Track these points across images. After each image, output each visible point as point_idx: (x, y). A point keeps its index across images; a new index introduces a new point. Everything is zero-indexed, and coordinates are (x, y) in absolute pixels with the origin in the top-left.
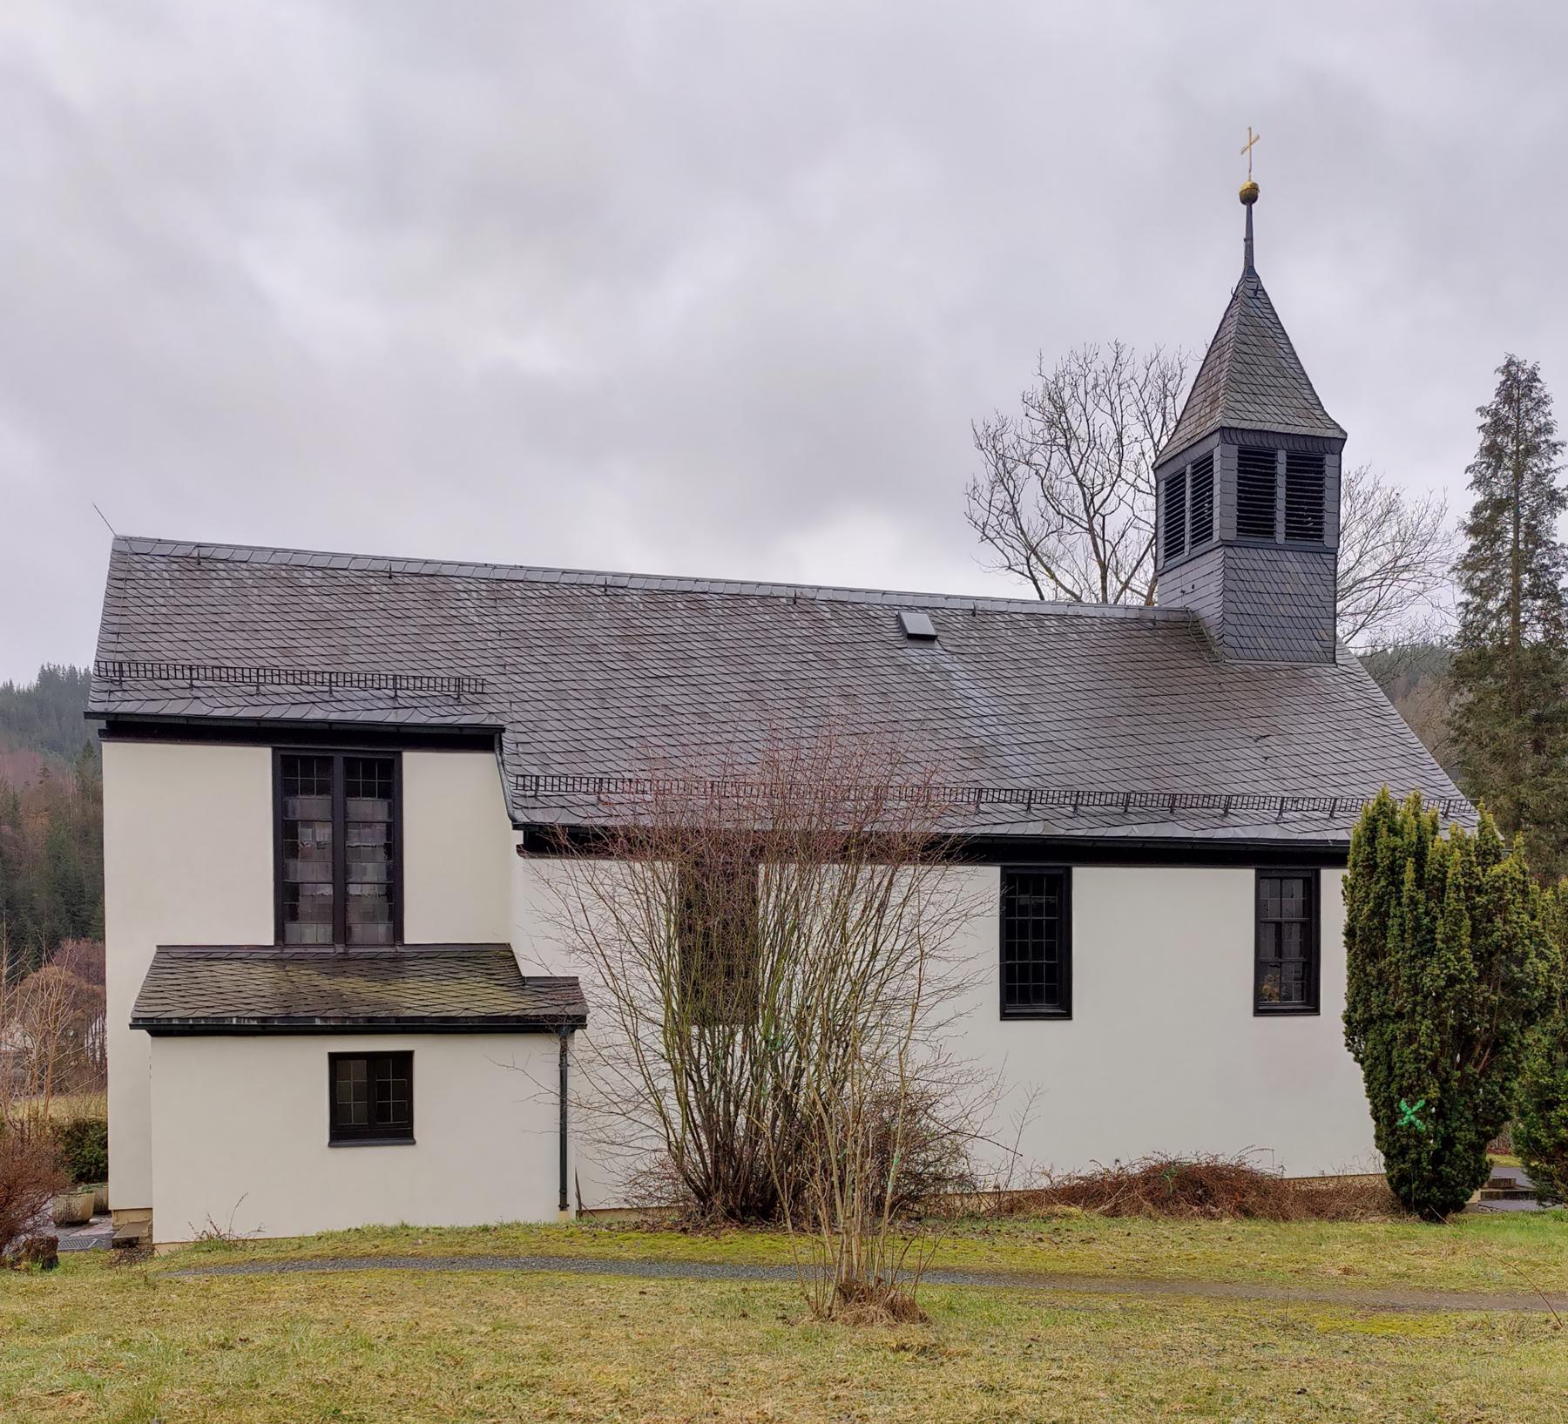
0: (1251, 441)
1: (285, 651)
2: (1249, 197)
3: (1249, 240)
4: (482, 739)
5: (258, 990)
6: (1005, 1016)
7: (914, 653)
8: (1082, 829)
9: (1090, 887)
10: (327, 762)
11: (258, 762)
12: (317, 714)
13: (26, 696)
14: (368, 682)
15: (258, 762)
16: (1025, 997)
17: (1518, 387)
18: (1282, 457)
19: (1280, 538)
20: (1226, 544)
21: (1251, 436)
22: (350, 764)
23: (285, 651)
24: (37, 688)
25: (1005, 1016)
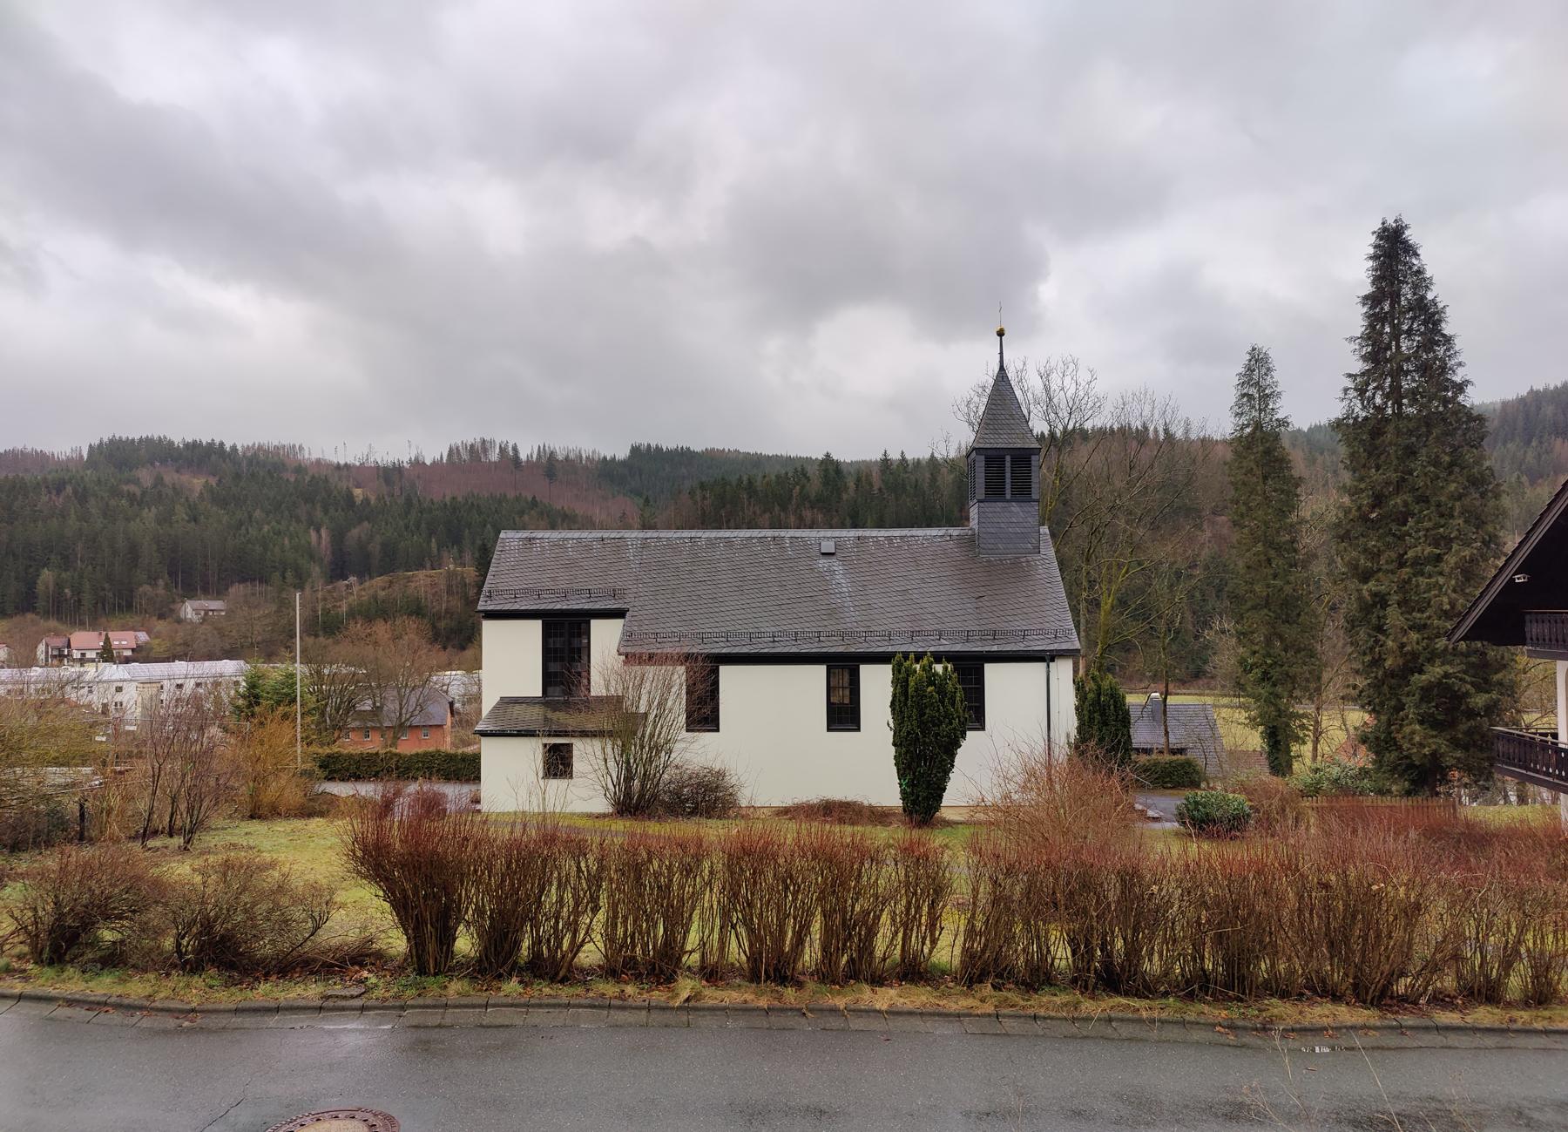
1: (553, 579)
2: (1001, 333)
4: (619, 614)
5: (534, 715)
6: (829, 730)
7: (823, 563)
11: (537, 625)
13: (623, 463)
14: (579, 592)
15: (537, 625)
16: (841, 722)
17: (1393, 248)
18: (1008, 458)
19: (1008, 496)
21: (590, 727)
23: (553, 579)
25: (829, 730)
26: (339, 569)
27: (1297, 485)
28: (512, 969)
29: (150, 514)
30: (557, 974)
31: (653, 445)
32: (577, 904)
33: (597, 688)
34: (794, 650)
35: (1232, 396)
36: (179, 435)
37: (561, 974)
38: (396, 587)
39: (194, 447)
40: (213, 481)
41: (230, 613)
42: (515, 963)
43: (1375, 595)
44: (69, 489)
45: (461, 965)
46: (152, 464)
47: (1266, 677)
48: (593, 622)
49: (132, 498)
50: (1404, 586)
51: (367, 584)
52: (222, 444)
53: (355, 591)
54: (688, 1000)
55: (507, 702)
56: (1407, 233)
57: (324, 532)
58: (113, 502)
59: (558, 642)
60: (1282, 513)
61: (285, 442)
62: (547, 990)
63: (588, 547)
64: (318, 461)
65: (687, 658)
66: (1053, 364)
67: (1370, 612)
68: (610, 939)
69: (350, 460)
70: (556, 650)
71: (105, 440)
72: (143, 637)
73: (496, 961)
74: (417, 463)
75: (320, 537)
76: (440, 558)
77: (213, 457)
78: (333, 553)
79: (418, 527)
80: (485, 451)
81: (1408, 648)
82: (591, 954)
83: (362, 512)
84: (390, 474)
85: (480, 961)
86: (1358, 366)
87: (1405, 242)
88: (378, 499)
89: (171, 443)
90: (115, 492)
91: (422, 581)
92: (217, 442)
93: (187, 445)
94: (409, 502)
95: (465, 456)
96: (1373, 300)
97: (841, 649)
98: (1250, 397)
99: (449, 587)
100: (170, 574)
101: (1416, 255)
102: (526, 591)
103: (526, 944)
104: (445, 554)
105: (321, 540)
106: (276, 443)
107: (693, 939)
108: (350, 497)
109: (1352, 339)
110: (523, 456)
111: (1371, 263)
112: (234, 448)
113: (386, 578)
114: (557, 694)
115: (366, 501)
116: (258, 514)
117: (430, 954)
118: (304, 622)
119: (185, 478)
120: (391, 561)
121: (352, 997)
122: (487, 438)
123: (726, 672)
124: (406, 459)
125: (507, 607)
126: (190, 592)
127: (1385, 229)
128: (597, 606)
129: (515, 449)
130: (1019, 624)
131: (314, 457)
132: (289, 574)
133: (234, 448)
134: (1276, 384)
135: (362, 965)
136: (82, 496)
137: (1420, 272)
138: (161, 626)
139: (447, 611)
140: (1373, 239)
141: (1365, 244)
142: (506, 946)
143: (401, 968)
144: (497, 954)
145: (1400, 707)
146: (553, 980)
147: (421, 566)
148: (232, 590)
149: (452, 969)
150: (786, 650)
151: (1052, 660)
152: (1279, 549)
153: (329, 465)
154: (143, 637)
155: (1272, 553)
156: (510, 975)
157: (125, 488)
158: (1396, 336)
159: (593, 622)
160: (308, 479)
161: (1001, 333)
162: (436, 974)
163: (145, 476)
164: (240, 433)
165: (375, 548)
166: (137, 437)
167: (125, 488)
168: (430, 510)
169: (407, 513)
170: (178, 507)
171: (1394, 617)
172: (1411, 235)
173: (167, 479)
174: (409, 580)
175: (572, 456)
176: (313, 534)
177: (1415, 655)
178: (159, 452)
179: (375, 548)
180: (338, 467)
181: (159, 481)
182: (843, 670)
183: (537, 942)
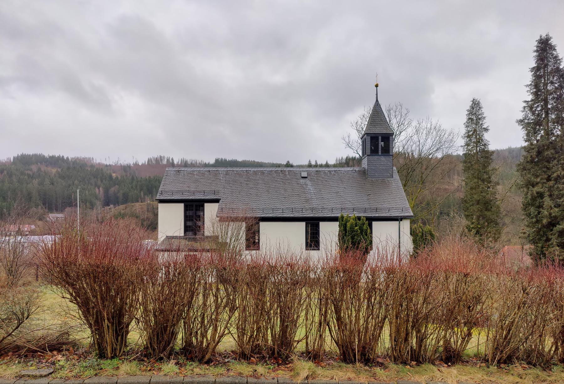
0: (372, 135)
1: (188, 187)
2: (377, 86)
3: (377, 94)
4: (217, 201)
7: (302, 181)
8: (321, 215)
10: (192, 206)
11: (182, 205)
12: (191, 198)
14: (199, 192)
15: (182, 205)
16: (311, 246)
17: (475, 106)
18: (380, 138)
19: (380, 154)
20: (368, 155)
22: (196, 206)
23: (188, 187)
24: (143, 165)
26: (107, 203)
27: (491, 155)
28: (170, 354)
29: (36, 182)
30: (203, 357)
31: (223, 158)
32: (217, 308)
33: (207, 233)
34: (292, 216)
35: (464, 119)
36: (47, 153)
37: (207, 357)
38: (128, 209)
39: (52, 157)
40: (59, 170)
41: (66, 219)
42: (172, 349)
43: (537, 193)
44: (5, 172)
45: (132, 351)
46: (37, 164)
47: (478, 232)
48: (206, 205)
49: (29, 176)
50: (550, 189)
51: (117, 208)
52: (63, 157)
53: (113, 210)
54: (307, 378)
55: (168, 238)
56: (552, 40)
57: (101, 189)
58: (22, 177)
59: (190, 213)
60: (485, 167)
61: (87, 157)
62: (197, 370)
63: (203, 174)
64: (99, 163)
65: (245, 219)
66: (391, 106)
67: (535, 202)
68: (242, 331)
69: (111, 163)
70: (190, 216)
71: (20, 155)
72: (33, 227)
73: (159, 348)
74: (136, 165)
75: (99, 191)
76: (144, 198)
77: (60, 161)
78: (104, 196)
79: (136, 187)
80: (161, 160)
81: (554, 214)
82: (228, 343)
83: (117, 182)
84: (126, 168)
85: (146, 348)
86: (530, 98)
87: (550, 45)
88: (121, 176)
89: (44, 156)
90: (22, 173)
91: (138, 206)
92: (61, 156)
93: (50, 157)
94: (133, 177)
95: (154, 162)
96: (536, 70)
97: (312, 215)
98: (472, 119)
99: (148, 209)
100: (43, 204)
101: (555, 49)
102: (178, 192)
103: (180, 336)
104: (146, 197)
105: (100, 192)
106: (83, 157)
107: (300, 333)
108: (111, 177)
109: (527, 86)
110: (175, 162)
111: (535, 54)
112: (68, 158)
113: (124, 206)
114: (190, 234)
115: (117, 178)
116: (76, 182)
117: (109, 343)
118: (80, 199)
119: (49, 169)
120: (126, 200)
121: (41, 376)
122: (162, 156)
123: (263, 225)
124: (132, 163)
125: (169, 198)
126: (51, 210)
127: (541, 40)
128: (207, 198)
129: (172, 159)
130: (386, 205)
131: (97, 162)
132: (88, 204)
133: (68, 158)
134: (483, 114)
135: (60, 351)
136: (10, 175)
137: (556, 57)
138: (40, 223)
139: (147, 218)
140: (536, 44)
141: (533, 45)
142: (166, 337)
143: (426, 317)
144: (159, 342)
145: (548, 240)
146: (201, 361)
147: (138, 201)
148: (66, 210)
149: (124, 354)
150: (288, 216)
151: (401, 220)
152: (483, 181)
153: (103, 165)
154: (33, 227)
155: (480, 183)
156: (169, 358)
157: (26, 172)
158: (546, 85)
159: (206, 205)
160: (95, 170)
162: (112, 358)
163: (34, 168)
164: (69, 153)
165: (120, 195)
166: (31, 154)
167: (26, 172)
168: (141, 181)
169: (132, 182)
170: (46, 179)
171: (547, 201)
172: (553, 42)
173: (42, 169)
174: (133, 206)
175: (193, 162)
176: (97, 190)
177: (556, 217)
178: (39, 159)
179: (120, 195)
180: (107, 166)
181: (39, 169)
182: (313, 226)
183: (189, 333)
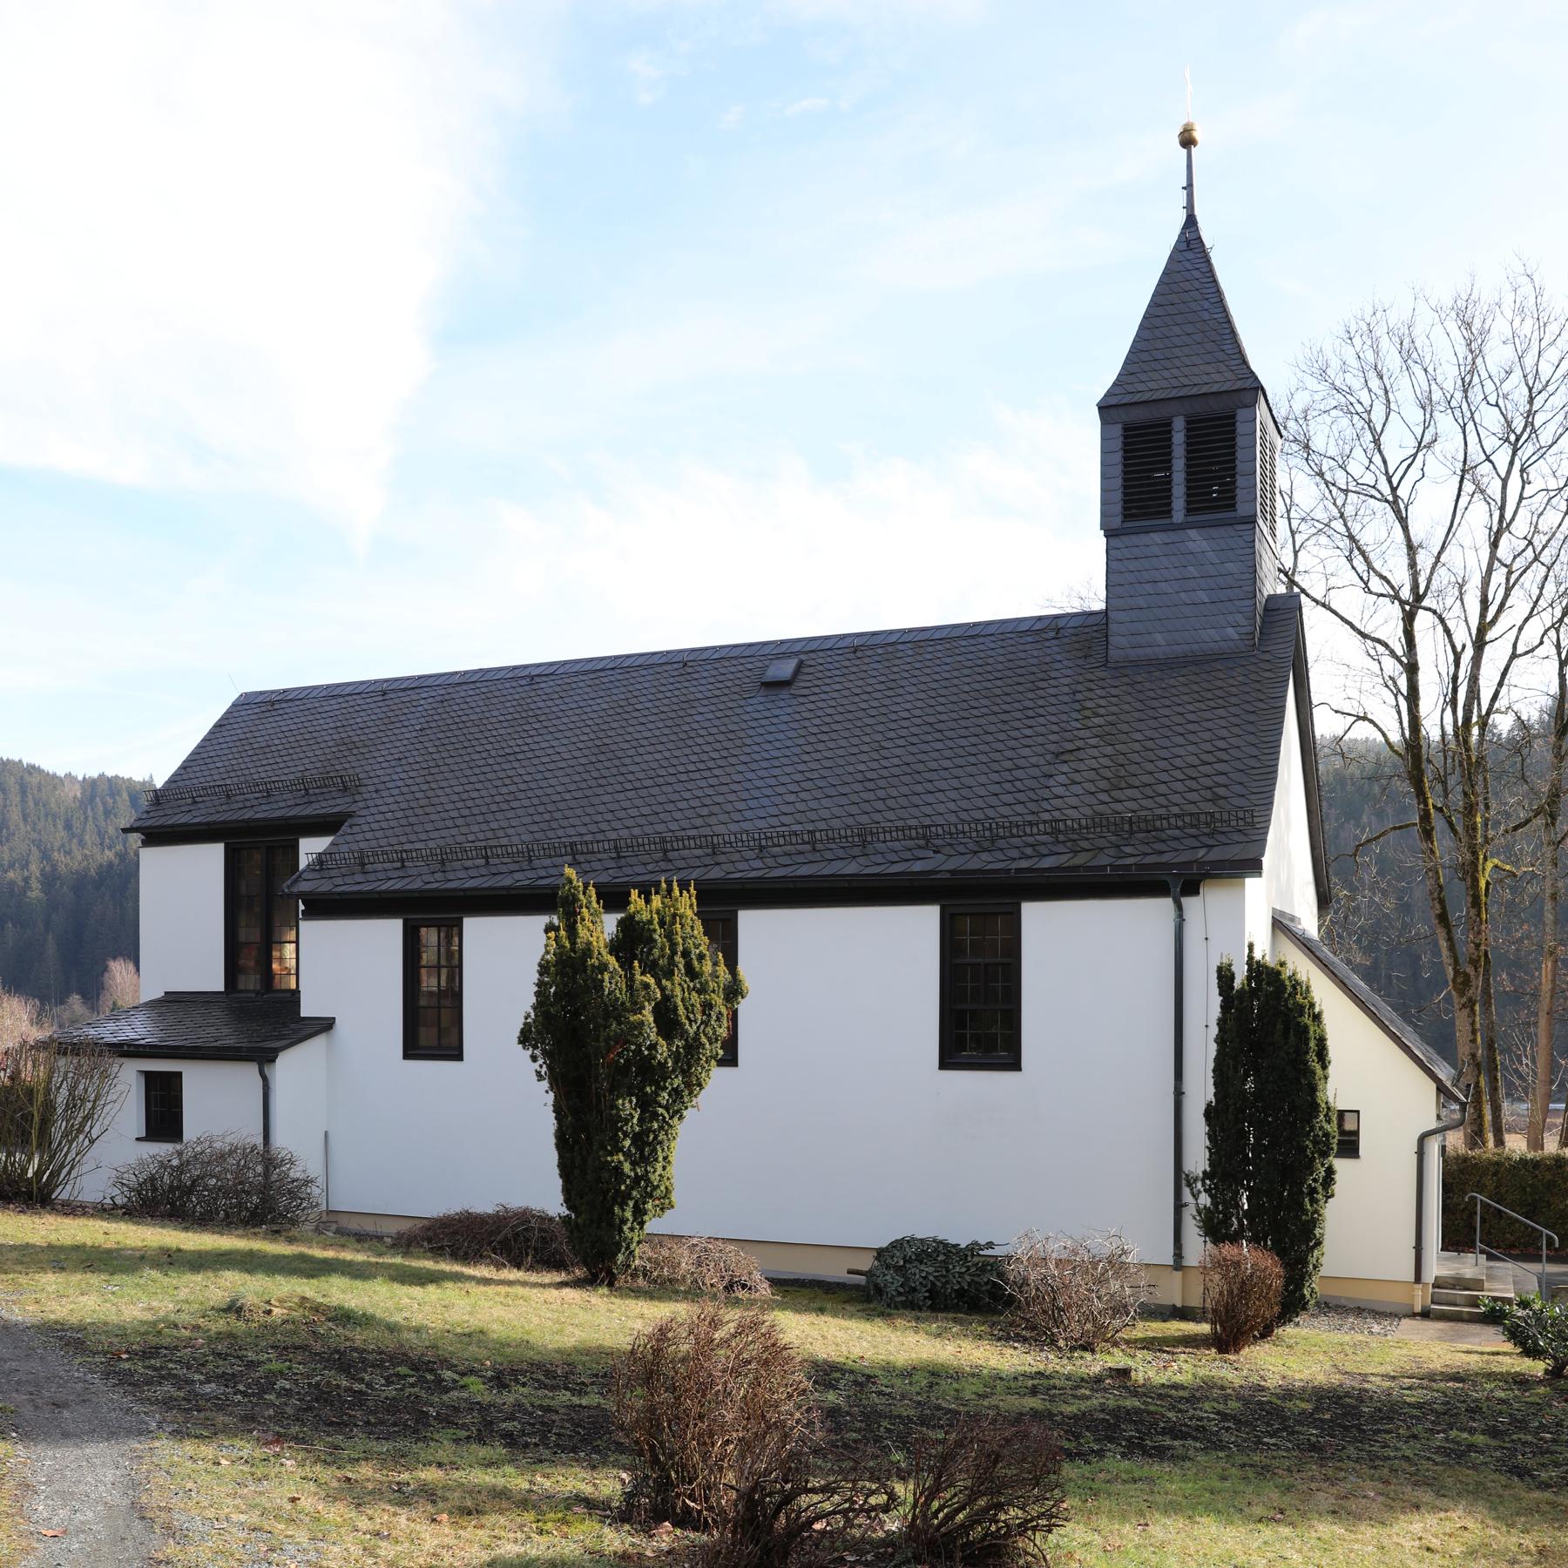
2: (1187, 141)
3: (1189, 187)
9: (1042, 923)
18: (1179, 424)
19: (1179, 515)
161: (1187, 141)
